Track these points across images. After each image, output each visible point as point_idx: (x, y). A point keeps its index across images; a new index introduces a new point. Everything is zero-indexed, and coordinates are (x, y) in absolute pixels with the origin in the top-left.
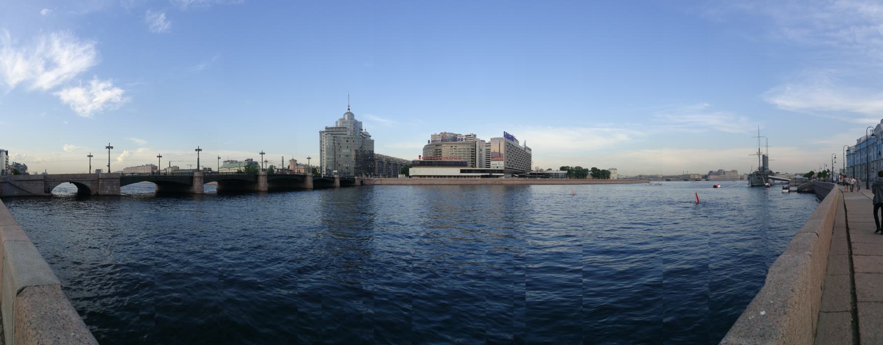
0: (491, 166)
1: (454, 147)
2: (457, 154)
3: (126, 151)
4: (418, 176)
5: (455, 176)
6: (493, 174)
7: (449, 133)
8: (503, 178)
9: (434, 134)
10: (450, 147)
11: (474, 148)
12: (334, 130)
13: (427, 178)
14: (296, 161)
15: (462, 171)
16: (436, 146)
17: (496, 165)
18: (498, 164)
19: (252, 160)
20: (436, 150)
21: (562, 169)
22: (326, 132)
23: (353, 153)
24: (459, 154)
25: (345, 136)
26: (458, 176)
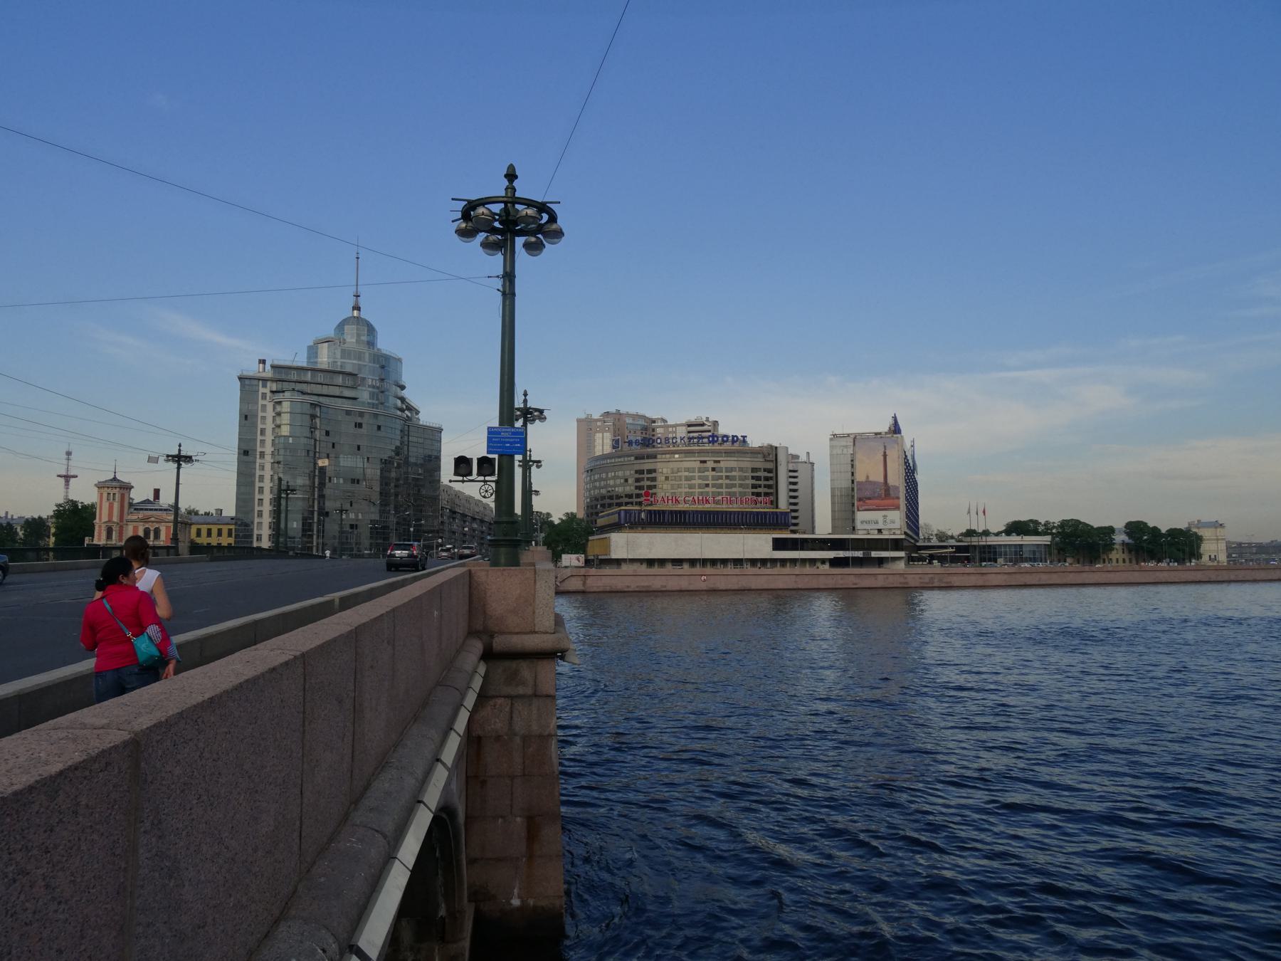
0: (859, 525)
1: (710, 465)
2: (720, 486)
3: (23, 534)
4: (641, 561)
5: (753, 562)
6: (874, 554)
7: (628, 415)
8: (901, 566)
9: (583, 416)
10: (697, 465)
11: (770, 466)
12: (309, 376)
13: (669, 568)
14: (128, 487)
15: (779, 544)
16: (637, 458)
18: (881, 520)
20: (637, 472)
21: (1017, 528)
22: (272, 380)
23: (374, 472)
25: (347, 405)
26: (764, 562)
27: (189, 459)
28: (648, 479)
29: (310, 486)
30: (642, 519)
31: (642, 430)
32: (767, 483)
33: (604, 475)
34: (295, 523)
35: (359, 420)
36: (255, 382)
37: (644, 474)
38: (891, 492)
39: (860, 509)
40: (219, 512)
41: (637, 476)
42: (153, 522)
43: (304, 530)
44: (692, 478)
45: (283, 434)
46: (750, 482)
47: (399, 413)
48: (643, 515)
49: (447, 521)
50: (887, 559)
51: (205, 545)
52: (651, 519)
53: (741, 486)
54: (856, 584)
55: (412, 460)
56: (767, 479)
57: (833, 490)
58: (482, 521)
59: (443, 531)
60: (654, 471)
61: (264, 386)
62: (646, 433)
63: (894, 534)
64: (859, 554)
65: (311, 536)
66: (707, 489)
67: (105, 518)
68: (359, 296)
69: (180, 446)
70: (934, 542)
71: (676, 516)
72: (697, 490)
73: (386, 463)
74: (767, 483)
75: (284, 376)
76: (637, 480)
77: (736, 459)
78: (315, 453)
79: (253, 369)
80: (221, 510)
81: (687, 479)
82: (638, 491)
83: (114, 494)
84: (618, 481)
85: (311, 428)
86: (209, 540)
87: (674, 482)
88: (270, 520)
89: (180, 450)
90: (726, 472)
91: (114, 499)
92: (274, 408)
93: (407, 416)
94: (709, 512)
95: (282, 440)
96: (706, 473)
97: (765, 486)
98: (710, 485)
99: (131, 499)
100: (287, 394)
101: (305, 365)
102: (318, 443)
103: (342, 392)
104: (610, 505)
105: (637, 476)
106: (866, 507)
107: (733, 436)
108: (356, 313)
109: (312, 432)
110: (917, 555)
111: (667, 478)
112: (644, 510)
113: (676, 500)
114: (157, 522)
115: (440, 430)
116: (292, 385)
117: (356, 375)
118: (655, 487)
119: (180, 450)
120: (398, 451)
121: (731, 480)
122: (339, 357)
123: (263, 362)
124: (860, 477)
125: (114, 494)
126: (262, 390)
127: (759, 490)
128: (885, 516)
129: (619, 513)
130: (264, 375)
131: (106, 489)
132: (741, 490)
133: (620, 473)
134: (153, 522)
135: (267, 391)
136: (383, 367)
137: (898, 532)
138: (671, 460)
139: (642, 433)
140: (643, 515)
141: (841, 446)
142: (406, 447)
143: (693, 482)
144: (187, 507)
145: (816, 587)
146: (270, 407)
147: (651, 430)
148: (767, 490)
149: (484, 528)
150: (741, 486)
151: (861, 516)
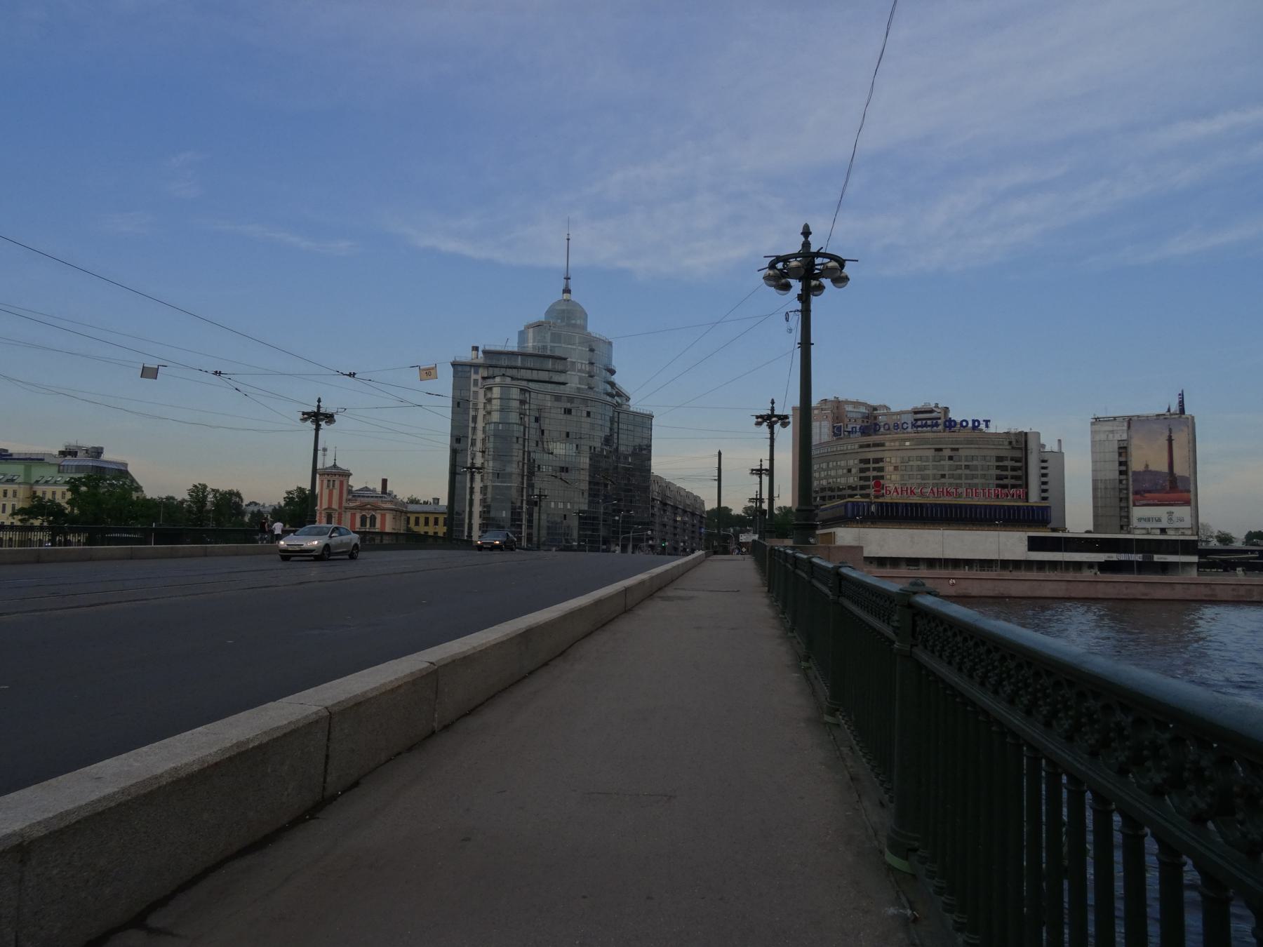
0: (1135, 522)
1: (947, 453)
2: (960, 477)
5: (1005, 564)
7: (847, 402)
10: (931, 453)
11: (1018, 454)
12: (519, 362)
14: (347, 475)
15: (1034, 544)
17: (1159, 520)
19: (98, 452)
20: (862, 461)
23: (585, 461)
24: (967, 477)
26: (1017, 564)
27: (330, 418)
28: (874, 469)
29: (519, 474)
30: (872, 512)
31: (863, 418)
32: (1014, 473)
33: (824, 466)
34: (504, 512)
35: (569, 405)
36: (467, 369)
37: (869, 463)
38: (1179, 484)
39: (1137, 504)
40: (436, 502)
41: (863, 466)
42: (369, 509)
43: (513, 520)
44: (925, 468)
45: (494, 420)
46: (995, 472)
47: (609, 399)
48: (873, 508)
49: (658, 514)
50: (1176, 564)
51: (422, 533)
52: (882, 512)
53: (984, 476)
54: (1146, 595)
55: (622, 449)
56: (1014, 469)
57: (1095, 482)
58: (693, 514)
59: (652, 523)
60: (881, 460)
61: (476, 373)
62: (867, 422)
63: (1183, 534)
64: (1137, 557)
65: (520, 526)
66: (943, 480)
67: (325, 505)
68: (569, 279)
69: (319, 401)
70: (1214, 544)
71: (912, 509)
72: (931, 482)
73: (595, 457)
74: (1014, 473)
75: (495, 361)
76: (862, 470)
77: (977, 446)
78: (524, 440)
79: (467, 356)
80: (438, 499)
81: (920, 468)
82: (862, 483)
83: (334, 481)
84: (840, 472)
85: (520, 414)
86: (426, 529)
87: (904, 473)
88: (480, 509)
89: (319, 407)
90: (966, 461)
91: (333, 486)
92: (485, 395)
93: (617, 402)
94: (961, 506)
95: (492, 426)
96: (942, 463)
97: (1012, 477)
98: (947, 476)
99: (350, 486)
100: (498, 380)
101: (516, 349)
102: (527, 429)
103: (552, 377)
104: (831, 498)
105: (863, 466)
106: (1144, 502)
107: (974, 421)
108: (566, 296)
109: (521, 418)
110: (1205, 560)
111: (896, 468)
112: (875, 502)
113: (912, 491)
114: (373, 510)
115: (650, 417)
116: (503, 371)
117: (565, 359)
118: (882, 477)
119: (319, 407)
120: (607, 440)
121: (971, 470)
122: (549, 341)
123: (476, 349)
124: (1136, 465)
125: (334, 481)
126: (474, 377)
127: (1005, 482)
128: (1170, 513)
129: (846, 505)
130: (475, 361)
131: (326, 476)
132: (983, 481)
133: (843, 463)
134: (369, 509)
135: (479, 377)
136: (592, 350)
137: (1189, 532)
138: (901, 448)
139: (863, 421)
140: (873, 508)
141: (1105, 431)
142: (616, 435)
143: (927, 472)
144: (409, 496)
145: (1094, 596)
146: (481, 392)
147: (873, 418)
148: (1013, 482)
149: (695, 522)
150: (984, 476)
151: (1137, 512)
